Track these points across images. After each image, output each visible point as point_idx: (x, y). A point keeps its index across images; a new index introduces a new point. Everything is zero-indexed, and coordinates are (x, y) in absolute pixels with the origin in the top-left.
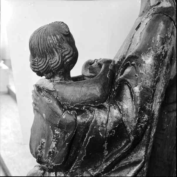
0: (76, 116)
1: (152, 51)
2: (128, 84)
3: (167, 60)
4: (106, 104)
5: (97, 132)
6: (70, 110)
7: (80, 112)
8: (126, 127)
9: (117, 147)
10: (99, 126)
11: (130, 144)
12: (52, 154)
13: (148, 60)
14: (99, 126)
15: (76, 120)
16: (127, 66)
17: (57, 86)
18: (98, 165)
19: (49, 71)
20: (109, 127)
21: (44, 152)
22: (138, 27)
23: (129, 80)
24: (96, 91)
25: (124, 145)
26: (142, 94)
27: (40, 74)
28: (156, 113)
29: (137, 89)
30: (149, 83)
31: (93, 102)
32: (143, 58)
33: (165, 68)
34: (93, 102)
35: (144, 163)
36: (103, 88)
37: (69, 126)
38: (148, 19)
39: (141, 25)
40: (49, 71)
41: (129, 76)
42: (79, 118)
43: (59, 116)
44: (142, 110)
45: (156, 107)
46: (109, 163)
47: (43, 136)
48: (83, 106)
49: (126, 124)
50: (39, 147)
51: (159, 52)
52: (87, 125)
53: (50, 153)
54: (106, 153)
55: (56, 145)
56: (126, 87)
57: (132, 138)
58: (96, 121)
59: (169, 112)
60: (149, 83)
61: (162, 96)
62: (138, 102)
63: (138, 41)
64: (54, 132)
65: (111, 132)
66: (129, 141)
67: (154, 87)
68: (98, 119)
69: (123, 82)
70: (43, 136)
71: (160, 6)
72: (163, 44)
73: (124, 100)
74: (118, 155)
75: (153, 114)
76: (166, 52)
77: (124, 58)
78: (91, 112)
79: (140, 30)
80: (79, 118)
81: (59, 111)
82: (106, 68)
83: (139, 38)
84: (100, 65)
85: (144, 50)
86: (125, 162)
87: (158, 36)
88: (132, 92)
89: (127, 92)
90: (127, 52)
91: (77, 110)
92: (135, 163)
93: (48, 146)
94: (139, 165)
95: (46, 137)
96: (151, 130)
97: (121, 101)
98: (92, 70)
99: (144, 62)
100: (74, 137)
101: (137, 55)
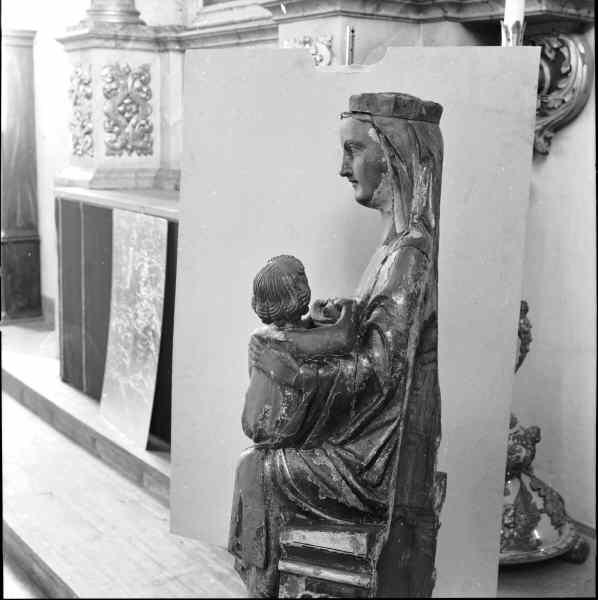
0: (318, 369)
1: (404, 291)
2: (377, 328)
3: (420, 299)
4: (352, 353)
5: (344, 386)
6: (309, 363)
7: (321, 365)
8: (378, 379)
9: (366, 405)
10: (346, 380)
11: (383, 399)
12: (280, 424)
13: (400, 300)
14: (346, 380)
15: (318, 373)
16: (373, 307)
17: (292, 334)
18: (341, 431)
19: (547, 85)
20: (359, 379)
21: (268, 422)
22: (385, 260)
23: (380, 325)
24: (341, 337)
25: (376, 402)
26: (395, 339)
27: (267, 321)
28: (411, 362)
29: (388, 334)
30: (401, 327)
31: (337, 352)
32: (394, 298)
33: (418, 308)
34: (337, 352)
35: (399, 421)
36: (350, 336)
37: (309, 382)
38: (397, 252)
39: (388, 260)
40: (547, 85)
41: (377, 319)
42: (321, 372)
43: (295, 371)
44: (395, 357)
45: (410, 354)
46: (358, 424)
47: (267, 401)
48: (323, 358)
49: (378, 374)
50: (261, 416)
51: (411, 291)
52: (331, 380)
53: (278, 422)
54: (353, 413)
55: (287, 411)
56: (375, 332)
57: (385, 391)
58: (342, 374)
59: (424, 364)
60: (401, 327)
61: (416, 341)
62: (391, 349)
63: (386, 278)
64: (284, 393)
65: (361, 385)
66: (382, 395)
67: (407, 331)
68: (345, 371)
69: (373, 326)
70: (267, 401)
71: (409, 236)
72: (416, 281)
73: (374, 348)
74: (370, 412)
75: (408, 363)
76: (419, 291)
77: (369, 297)
78: (336, 363)
79: (388, 264)
80: (321, 372)
81: (295, 365)
82: (348, 310)
83: (386, 274)
84: (339, 307)
85: (394, 288)
86: (376, 423)
87: (410, 272)
88: (383, 338)
89: (376, 336)
90: (372, 292)
91: (318, 363)
92: (389, 423)
93: (276, 412)
94: (395, 424)
95: (272, 402)
96: (405, 381)
97: (371, 348)
98: (327, 313)
99: (395, 303)
100: (315, 396)
101: (387, 295)
